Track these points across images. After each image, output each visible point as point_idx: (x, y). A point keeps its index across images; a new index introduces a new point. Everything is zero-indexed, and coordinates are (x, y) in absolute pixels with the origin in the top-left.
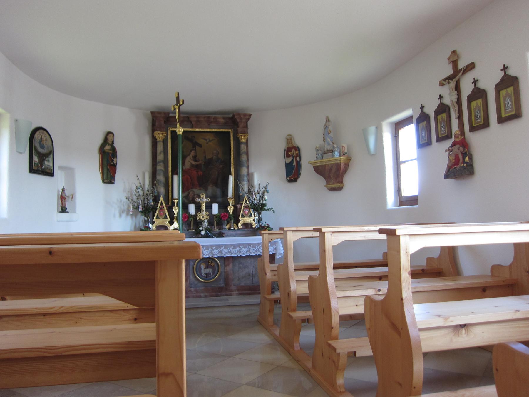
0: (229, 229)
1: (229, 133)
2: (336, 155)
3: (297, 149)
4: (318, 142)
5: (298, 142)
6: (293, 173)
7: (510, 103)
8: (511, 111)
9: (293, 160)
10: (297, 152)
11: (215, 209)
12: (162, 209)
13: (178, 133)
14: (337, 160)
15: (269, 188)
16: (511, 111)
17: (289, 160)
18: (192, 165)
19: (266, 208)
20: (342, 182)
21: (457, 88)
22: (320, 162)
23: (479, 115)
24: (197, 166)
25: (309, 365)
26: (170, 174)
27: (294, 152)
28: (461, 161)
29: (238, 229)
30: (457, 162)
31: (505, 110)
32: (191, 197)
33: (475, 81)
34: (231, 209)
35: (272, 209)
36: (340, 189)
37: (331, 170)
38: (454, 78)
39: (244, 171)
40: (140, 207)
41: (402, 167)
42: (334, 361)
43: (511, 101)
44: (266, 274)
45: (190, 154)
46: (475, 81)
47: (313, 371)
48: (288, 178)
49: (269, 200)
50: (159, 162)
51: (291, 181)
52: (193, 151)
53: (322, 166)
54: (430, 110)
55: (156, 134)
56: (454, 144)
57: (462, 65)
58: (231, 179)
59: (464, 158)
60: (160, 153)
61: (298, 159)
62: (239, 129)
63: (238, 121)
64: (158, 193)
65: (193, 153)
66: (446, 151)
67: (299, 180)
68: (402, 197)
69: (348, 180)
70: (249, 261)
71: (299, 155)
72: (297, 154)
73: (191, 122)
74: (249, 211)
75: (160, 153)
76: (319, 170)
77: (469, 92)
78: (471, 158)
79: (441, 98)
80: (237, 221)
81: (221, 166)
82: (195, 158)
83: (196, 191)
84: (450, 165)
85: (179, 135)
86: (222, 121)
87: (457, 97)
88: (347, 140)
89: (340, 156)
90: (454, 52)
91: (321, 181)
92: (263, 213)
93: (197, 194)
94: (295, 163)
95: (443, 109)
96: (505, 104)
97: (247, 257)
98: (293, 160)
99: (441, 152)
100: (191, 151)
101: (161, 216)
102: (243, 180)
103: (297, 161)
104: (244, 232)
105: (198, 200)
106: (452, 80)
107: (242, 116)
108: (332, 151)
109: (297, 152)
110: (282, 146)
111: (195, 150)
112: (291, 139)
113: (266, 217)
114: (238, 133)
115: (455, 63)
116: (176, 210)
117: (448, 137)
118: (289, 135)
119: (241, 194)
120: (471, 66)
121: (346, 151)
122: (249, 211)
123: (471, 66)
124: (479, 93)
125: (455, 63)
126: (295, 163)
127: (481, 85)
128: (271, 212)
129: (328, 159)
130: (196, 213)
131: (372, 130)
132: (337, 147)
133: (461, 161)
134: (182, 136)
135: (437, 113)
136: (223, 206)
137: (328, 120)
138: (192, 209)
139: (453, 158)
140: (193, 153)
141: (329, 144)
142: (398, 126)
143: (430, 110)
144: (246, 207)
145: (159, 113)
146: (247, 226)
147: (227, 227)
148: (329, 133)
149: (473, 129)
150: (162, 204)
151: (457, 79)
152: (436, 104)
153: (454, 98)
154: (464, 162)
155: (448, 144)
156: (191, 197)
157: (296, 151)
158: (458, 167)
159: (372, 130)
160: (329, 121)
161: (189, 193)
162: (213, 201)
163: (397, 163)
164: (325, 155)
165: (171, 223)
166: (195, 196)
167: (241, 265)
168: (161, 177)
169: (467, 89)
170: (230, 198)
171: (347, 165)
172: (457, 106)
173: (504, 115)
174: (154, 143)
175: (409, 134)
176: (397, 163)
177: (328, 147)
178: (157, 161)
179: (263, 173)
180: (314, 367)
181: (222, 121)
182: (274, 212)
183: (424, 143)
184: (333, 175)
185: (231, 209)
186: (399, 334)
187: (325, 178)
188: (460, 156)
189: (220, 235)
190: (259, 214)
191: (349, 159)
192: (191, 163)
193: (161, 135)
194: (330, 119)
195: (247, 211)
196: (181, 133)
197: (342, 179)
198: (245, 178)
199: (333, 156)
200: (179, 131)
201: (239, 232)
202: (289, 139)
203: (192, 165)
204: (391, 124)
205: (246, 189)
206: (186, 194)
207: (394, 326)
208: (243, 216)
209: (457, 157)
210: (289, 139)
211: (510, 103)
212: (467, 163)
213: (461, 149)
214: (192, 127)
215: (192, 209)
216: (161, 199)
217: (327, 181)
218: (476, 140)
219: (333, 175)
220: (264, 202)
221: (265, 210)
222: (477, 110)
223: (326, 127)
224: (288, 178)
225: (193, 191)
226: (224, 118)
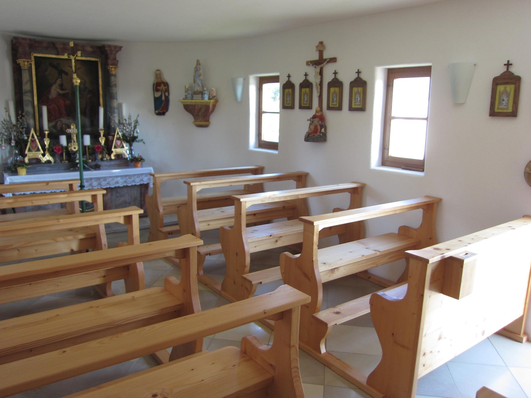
0: (102, 159)
1: (96, 62)
2: (206, 97)
3: (166, 84)
4: (188, 81)
5: (167, 78)
6: (161, 106)
7: (359, 99)
8: (358, 105)
9: (162, 95)
10: (166, 87)
11: (87, 140)
12: (33, 141)
13: (75, 84)
14: (206, 102)
15: (139, 119)
16: (358, 105)
17: (158, 95)
18: (59, 94)
19: (137, 139)
20: (208, 120)
21: (321, 73)
22: (189, 101)
23: (335, 100)
24: (64, 95)
25: (219, 288)
26: (36, 103)
27: (163, 87)
28: (319, 131)
29: (111, 159)
30: (316, 131)
31: (355, 102)
32: (59, 127)
33: (335, 73)
34: (102, 141)
35: (142, 140)
36: (206, 126)
37: (200, 109)
38: (319, 63)
39: (115, 104)
40: (13, 141)
41: (264, 116)
42: (247, 288)
43: (360, 97)
44: (159, 211)
45: (56, 82)
46: (335, 73)
47: (223, 293)
48: (157, 112)
49: (139, 132)
50: (26, 92)
51: (159, 114)
52: (59, 79)
53: (192, 105)
54: (297, 81)
55: (20, 61)
56: (314, 117)
57: (326, 56)
58: (101, 111)
59: (321, 129)
60: (27, 83)
61: (167, 94)
62: (110, 61)
63: (109, 52)
64: (28, 125)
65: (59, 81)
66: (308, 120)
67: (167, 114)
68: (262, 141)
69: (214, 119)
70: (125, 190)
71: (167, 90)
72: (166, 89)
73: (56, 49)
74: (121, 142)
75: (27, 83)
76: (188, 108)
77: (330, 80)
78: (325, 130)
79: (306, 75)
80: (110, 152)
81: (89, 96)
82: (61, 87)
83: (65, 120)
84: (310, 132)
85: (76, 86)
86: (89, 49)
87: (320, 80)
88: (215, 82)
89: (209, 99)
90: (321, 43)
91: (189, 118)
92: (135, 144)
93: (66, 124)
94: (163, 98)
95: (306, 84)
96: (355, 99)
97: (124, 187)
98: (162, 95)
99: (303, 119)
100: (57, 79)
101: (33, 148)
102: (114, 113)
103: (165, 96)
104: (117, 162)
105: (69, 131)
106: (318, 65)
107: (113, 48)
108: (202, 93)
109: (166, 87)
110: (151, 80)
111: (62, 78)
112: (160, 74)
113: (138, 150)
114: (108, 65)
115: (321, 53)
116: (47, 142)
117: (310, 107)
118: (158, 70)
119: (113, 126)
120: (333, 60)
121: (215, 94)
122: (121, 142)
123: (333, 60)
124: (336, 83)
125: (321, 53)
126: (163, 98)
127: (340, 77)
128: (141, 143)
129: (197, 100)
130: (68, 143)
131: (241, 80)
132: (207, 90)
133: (319, 131)
134: (80, 87)
135: (302, 86)
136: (95, 137)
137: (198, 63)
138: (63, 140)
139: (312, 127)
140: (59, 81)
141: (198, 85)
142: (262, 81)
143: (297, 81)
144: (118, 139)
145: (24, 39)
146: (119, 156)
147: (100, 156)
148: (199, 76)
149: (329, 108)
150: (33, 136)
151: (322, 65)
152: (302, 79)
153: (318, 81)
154: (320, 132)
155: (310, 114)
156: (59, 127)
157: (165, 86)
158: (316, 135)
159: (241, 80)
160: (200, 64)
161: (57, 123)
162: (84, 133)
163: (260, 113)
164: (195, 96)
165: (44, 155)
166: (64, 126)
167: (118, 195)
168: (28, 108)
169: (328, 77)
170: (101, 130)
171: (214, 106)
172: (319, 87)
173: (353, 106)
174: (17, 71)
175: (272, 92)
176: (260, 113)
177: (198, 89)
178: (24, 91)
179: (131, 105)
180: (223, 288)
181: (89, 49)
182: (144, 143)
183: (287, 105)
184: (201, 114)
185: (102, 141)
186: (309, 280)
187: (193, 115)
188: (319, 127)
189: (97, 167)
190: (131, 146)
191: (217, 101)
192: (58, 92)
193: (26, 63)
194: (201, 62)
195: (119, 142)
196: (78, 84)
197: (209, 118)
198: (116, 110)
199: (203, 98)
200: (77, 82)
201: (113, 163)
202: (158, 74)
203: (59, 94)
204: (257, 77)
205: (117, 121)
206: (53, 124)
207: (306, 275)
208: (115, 147)
209: (316, 127)
210: (158, 74)
211: (359, 99)
212: (323, 133)
213: (320, 122)
214: (58, 54)
215: (63, 140)
216: (32, 131)
217: (195, 118)
218: (331, 117)
219: (201, 114)
220: (135, 135)
221: (137, 141)
222: (334, 95)
223: (197, 70)
224: (157, 112)
225: (61, 121)
226: (92, 47)
